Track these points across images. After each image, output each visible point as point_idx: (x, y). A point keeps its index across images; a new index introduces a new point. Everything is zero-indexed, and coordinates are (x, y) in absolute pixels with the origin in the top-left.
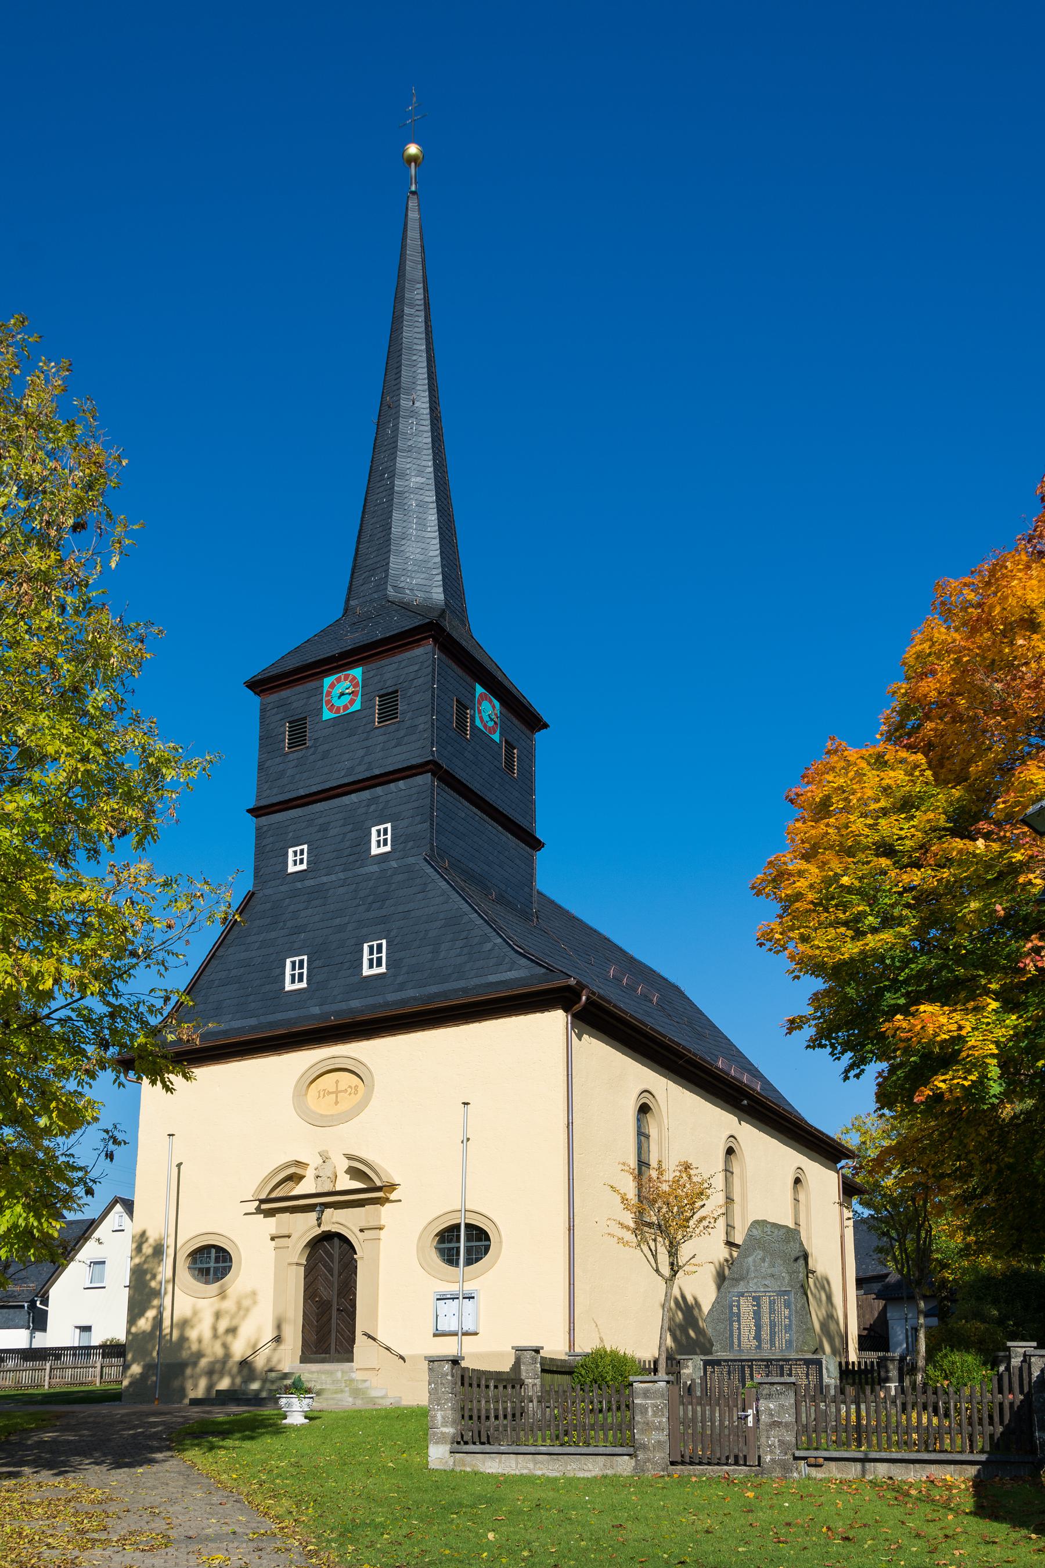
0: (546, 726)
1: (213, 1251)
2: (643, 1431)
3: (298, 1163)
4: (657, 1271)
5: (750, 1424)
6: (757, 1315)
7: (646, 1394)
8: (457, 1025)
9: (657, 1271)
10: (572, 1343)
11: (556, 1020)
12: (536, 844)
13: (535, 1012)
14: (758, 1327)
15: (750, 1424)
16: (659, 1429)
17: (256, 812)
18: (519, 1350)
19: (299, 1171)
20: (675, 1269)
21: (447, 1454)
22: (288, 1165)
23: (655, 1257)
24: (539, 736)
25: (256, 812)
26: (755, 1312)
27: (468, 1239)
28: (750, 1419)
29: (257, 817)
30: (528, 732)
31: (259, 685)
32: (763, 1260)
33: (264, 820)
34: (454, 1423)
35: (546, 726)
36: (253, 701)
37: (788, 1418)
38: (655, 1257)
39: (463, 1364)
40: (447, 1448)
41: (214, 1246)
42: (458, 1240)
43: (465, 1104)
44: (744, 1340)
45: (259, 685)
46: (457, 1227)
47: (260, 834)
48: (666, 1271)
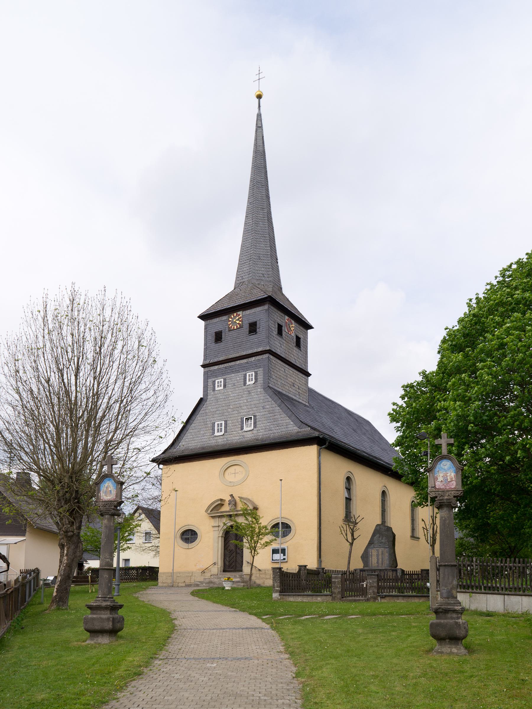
0: (311, 375)
1: (190, 531)
2: (334, 589)
3: (221, 500)
4: (347, 540)
5: (365, 586)
6: (378, 555)
7: (336, 578)
8: (279, 449)
9: (347, 540)
10: (349, 568)
11: (313, 449)
12: (308, 375)
13: (307, 445)
14: (378, 559)
15: (365, 586)
16: (339, 588)
17: (203, 366)
18: (300, 566)
19: (223, 503)
20: (353, 539)
21: (278, 596)
22: (217, 501)
23: (346, 535)
24: (309, 331)
25: (203, 366)
26: (377, 554)
27: (283, 528)
28: (365, 585)
29: (204, 368)
30: (305, 331)
31: (203, 317)
32: (379, 537)
33: (207, 369)
34: (280, 587)
35: (311, 375)
36: (202, 323)
37: (375, 584)
38: (346, 535)
39: (283, 570)
40: (278, 594)
41: (191, 530)
42: (279, 528)
43: (281, 480)
44: (373, 563)
45: (203, 317)
46: (278, 523)
47: (205, 373)
48: (350, 540)
